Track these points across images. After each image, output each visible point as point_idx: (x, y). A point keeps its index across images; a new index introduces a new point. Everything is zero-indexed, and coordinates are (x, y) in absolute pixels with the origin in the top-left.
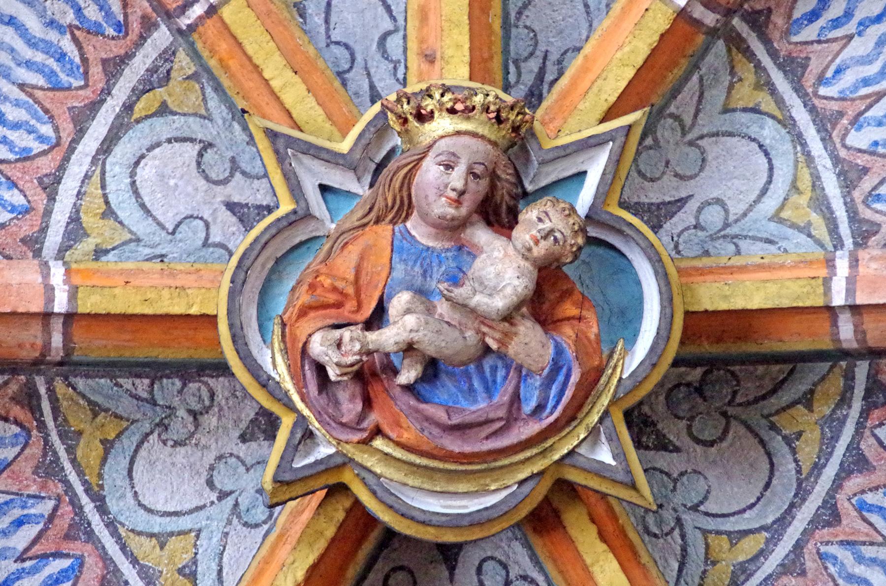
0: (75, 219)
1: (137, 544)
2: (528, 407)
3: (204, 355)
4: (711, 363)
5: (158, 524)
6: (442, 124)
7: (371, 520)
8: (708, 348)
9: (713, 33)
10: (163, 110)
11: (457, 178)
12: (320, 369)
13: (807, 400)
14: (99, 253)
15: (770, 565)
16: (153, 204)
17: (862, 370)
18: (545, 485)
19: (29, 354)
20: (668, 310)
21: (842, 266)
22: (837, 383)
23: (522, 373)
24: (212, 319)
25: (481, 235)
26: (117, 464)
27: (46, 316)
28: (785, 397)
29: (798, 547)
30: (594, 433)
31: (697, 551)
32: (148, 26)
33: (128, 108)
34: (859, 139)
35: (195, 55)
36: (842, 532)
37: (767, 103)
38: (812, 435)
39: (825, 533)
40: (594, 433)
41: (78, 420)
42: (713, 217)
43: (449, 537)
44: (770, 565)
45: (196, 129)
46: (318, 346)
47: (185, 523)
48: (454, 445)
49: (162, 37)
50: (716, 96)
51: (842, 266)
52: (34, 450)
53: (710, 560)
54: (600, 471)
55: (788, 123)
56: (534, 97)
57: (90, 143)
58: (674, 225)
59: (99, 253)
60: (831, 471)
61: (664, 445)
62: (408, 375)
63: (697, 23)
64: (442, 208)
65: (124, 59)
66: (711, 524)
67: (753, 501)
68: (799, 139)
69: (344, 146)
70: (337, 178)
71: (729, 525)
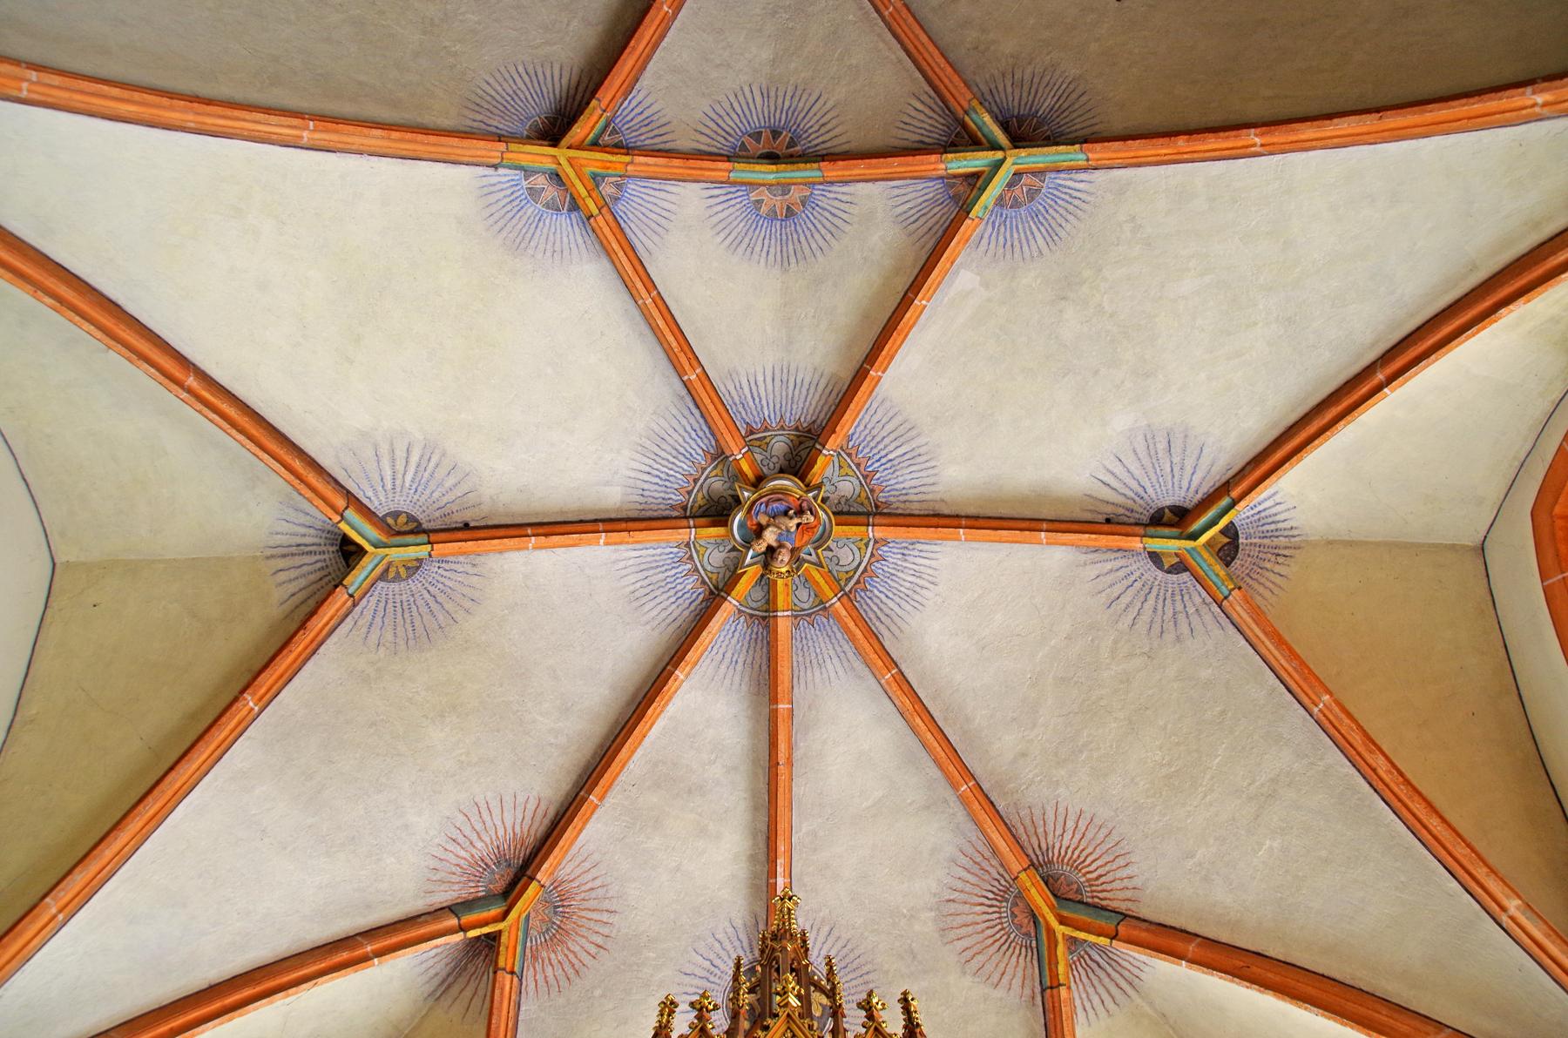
0: (867, 547)
1: (852, 474)
2: (763, 505)
3: (838, 517)
4: (722, 515)
5: (848, 478)
6: (784, 570)
7: (800, 479)
8: (723, 518)
9: (722, 590)
10: (847, 572)
11: (780, 558)
12: (812, 513)
13: (700, 507)
14: (861, 540)
15: (709, 469)
16: (782, 652)
17: (688, 514)
18: (760, 486)
19: (877, 517)
21: (692, 537)
22: (694, 511)
23: (765, 513)
24: (837, 525)
25: (775, 544)
26: (857, 492)
27: (873, 525)
28: (705, 508)
30: (749, 499)
32: (850, 591)
33: (855, 573)
34: (689, 566)
35: (840, 585)
37: (709, 574)
38: (699, 499)
40: (749, 499)
41: (866, 502)
42: (721, 549)
43: (782, 475)
44: (709, 469)
45: (838, 568)
46: (812, 519)
48: (780, 496)
49: (847, 589)
50: (721, 576)
51: (692, 537)
52: (875, 495)
53: (722, 470)
54: (747, 490)
55: (705, 570)
56: (762, 576)
57: (863, 565)
58: (730, 547)
59: (861, 540)
60: (695, 491)
61: (732, 496)
62: (791, 512)
63: (820, 444)
64: (784, 551)
65: (856, 584)
68: (702, 566)
69: (806, 565)
70: (808, 557)
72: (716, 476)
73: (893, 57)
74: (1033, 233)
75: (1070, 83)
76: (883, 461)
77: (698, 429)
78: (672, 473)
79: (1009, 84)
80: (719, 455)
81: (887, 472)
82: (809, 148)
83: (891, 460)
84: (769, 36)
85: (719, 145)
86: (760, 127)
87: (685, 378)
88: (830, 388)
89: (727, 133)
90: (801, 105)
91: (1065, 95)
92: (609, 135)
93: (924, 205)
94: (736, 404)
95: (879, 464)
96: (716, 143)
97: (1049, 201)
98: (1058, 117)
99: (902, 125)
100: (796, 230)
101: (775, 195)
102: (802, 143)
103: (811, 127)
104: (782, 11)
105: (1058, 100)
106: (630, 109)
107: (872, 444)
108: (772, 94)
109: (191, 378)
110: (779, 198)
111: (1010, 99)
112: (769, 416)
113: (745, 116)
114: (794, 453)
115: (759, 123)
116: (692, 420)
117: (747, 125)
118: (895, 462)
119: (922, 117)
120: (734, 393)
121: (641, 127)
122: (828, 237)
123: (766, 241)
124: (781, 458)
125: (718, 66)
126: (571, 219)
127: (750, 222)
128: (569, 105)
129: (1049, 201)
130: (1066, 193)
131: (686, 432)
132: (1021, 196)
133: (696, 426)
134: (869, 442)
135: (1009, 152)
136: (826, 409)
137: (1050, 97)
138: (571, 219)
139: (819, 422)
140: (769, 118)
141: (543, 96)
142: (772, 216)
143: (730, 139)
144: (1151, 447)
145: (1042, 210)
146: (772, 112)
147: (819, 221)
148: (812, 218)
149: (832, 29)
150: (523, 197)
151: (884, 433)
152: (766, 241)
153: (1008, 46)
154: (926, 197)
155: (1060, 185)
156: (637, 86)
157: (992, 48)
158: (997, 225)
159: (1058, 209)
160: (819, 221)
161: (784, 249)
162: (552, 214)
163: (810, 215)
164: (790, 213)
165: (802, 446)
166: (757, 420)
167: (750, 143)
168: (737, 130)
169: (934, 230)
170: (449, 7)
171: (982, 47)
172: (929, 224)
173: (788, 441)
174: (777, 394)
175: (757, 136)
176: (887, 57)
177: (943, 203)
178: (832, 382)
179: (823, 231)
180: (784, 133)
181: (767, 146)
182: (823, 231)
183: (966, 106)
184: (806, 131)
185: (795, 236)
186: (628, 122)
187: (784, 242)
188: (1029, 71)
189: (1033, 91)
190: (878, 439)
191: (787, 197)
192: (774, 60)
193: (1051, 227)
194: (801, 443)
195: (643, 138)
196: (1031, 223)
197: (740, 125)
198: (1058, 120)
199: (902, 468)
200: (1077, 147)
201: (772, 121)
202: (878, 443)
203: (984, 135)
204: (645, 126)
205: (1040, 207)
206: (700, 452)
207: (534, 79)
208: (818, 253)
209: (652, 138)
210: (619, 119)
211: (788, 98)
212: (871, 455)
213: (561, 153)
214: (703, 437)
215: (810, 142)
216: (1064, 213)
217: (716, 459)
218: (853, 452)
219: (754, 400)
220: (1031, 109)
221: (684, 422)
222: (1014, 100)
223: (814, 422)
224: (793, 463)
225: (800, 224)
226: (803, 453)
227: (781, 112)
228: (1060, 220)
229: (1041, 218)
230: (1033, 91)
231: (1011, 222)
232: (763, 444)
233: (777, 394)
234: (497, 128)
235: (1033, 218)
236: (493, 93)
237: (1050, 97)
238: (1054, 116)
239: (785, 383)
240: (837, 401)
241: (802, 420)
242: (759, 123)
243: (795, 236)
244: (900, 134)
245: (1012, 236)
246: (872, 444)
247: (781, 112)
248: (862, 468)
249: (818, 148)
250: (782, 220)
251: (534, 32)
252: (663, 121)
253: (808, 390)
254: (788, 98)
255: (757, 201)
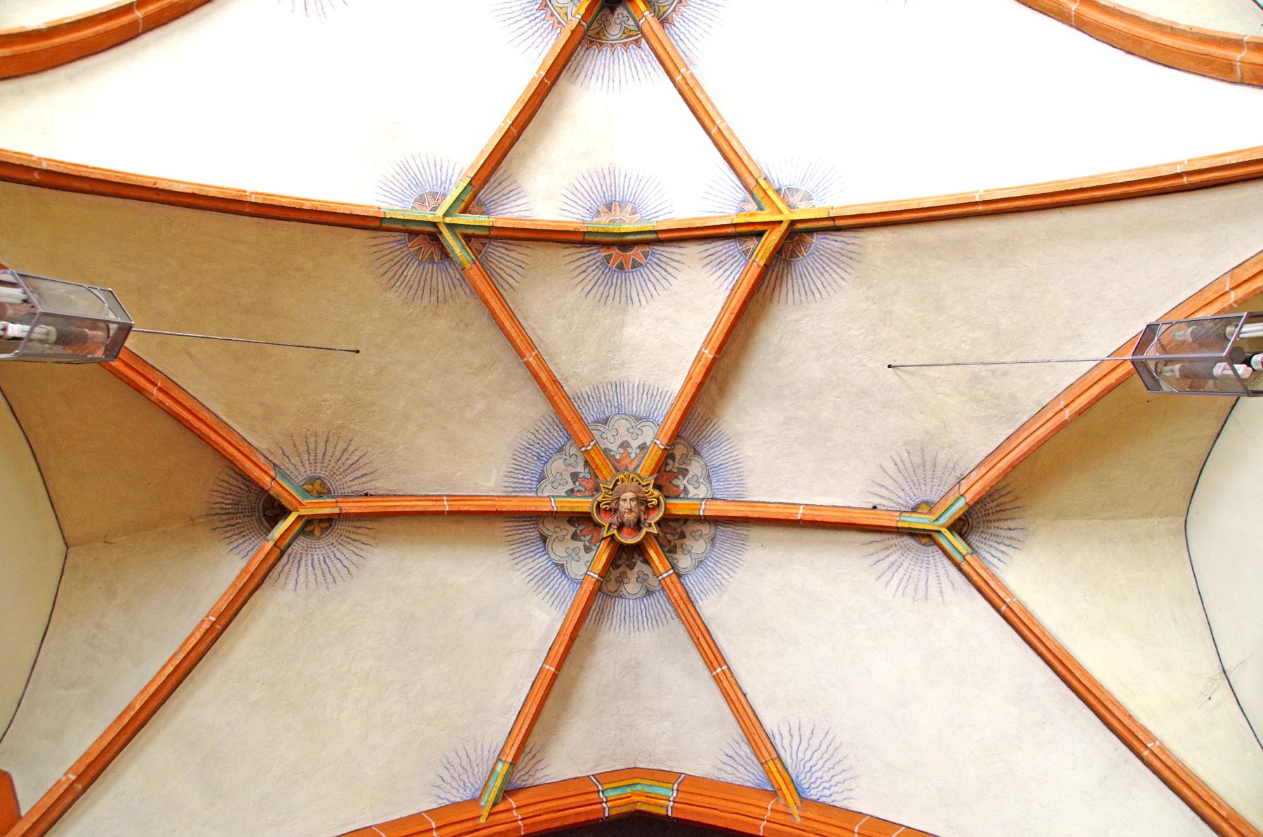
5: (560, 5)
20: (531, 368)
29: (675, 8)
31: (657, 9)
36: (682, 4)
39: (679, 5)
47: (565, 5)
53: (659, 10)
66: (659, 5)
67: (997, 559)
71: (663, 4)
72: (664, 6)
73: (530, 323)
74: (420, 172)
75: (394, 286)
76: (533, 17)
77: (679, 41)
78: (700, 7)
79: (441, 291)
80: (664, 21)
81: (530, 9)
82: (595, 254)
83: (527, 17)
84: (626, 345)
85: (664, 254)
86: (633, 272)
87: (703, 350)
88: (575, 74)
89: (659, 265)
90: (601, 289)
91: (397, 276)
92: (750, 249)
93: (505, 202)
94: (649, 61)
95: (536, 15)
96: (667, 255)
97: (408, 193)
98: (403, 258)
99: (523, 265)
100: (604, 193)
101: (621, 219)
102: (600, 258)
103: (593, 271)
104: (617, 366)
105: (402, 273)
106: (734, 273)
107: (542, 30)
108: (623, 299)
109: (1073, 9)
110: (618, 218)
111: (439, 279)
112: (623, 54)
113: (645, 280)
114: (602, 26)
115: (633, 275)
116: (683, 47)
117: (643, 273)
118: (523, 16)
119: (508, 271)
120: (651, 70)
121: (725, 260)
122: (579, 187)
123: (627, 185)
124: (613, 23)
125: (666, 318)
126: (779, 183)
127: (639, 198)
128: (781, 270)
129: (408, 193)
130: (395, 196)
131: (688, 38)
132: (430, 200)
133: (680, 43)
134: (544, 32)
135: (441, 220)
136: (579, 58)
137: (409, 276)
138: (779, 183)
139: (584, 49)
140: (626, 280)
141: (801, 275)
142: (622, 205)
143: (656, 261)
144: (320, 8)
145: (412, 187)
146: (623, 285)
147: (586, 199)
148: (592, 201)
149: (577, 350)
150: (815, 194)
151: (532, 39)
152: (627, 185)
153: (442, 325)
154: (503, 207)
155: (400, 202)
156: (728, 292)
157: (454, 324)
158: (448, 182)
159: (400, 186)
160: (586, 199)
161: (613, 180)
162: (794, 185)
163: (594, 204)
164: (609, 206)
165: (596, 31)
166: (632, 51)
167: (641, 259)
168: (650, 268)
169: (497, 183)
170: (872, 338)
171: (462, 326)
172: (500, 188)
173: (608, 35)
174: (617, 72)
175: (636, 265)
176: (536, 322)
177: (490, 202)
178: (574, 78)
179: (583, 191)
180: (614, 267)
181: (627, 258)
182: (583, 191)
183: (474, 266)
184: (597, 268)
185: (604, 189)
186: (735, 262)
187: (613, 185)
188: (426, 301)
189: (422, 283)
190: (538, 34)
191: (612, 218)
192: (623, 326)
193: (406, 174)
194: (598, 33)
195: (724, 251)
196: (421, 180)
197: (648, 273)
198: (402, 255)
199: (518, 11)
200: (388, 216)
201: (623, 278)
202: (537, 31)
203: (461, 241)
204: (722, 262)
205: (414, 189)
206: (676, 24)
207: (807, 289)
208: (587, 176)
209: (717, 252)
210: (742, 263)
211: (611, 296)
212: (542, 22)
213: (787, 216)
214: (674, 35)
215: (594, 259)
216: (396, 182)
217: (664, 19)
218: (556, 25)
219: (635, 66)
220: (424, 268)
221: (689, 45)
222: (439, 277)
223: (588, 49)
224: (604, 19)
225: (601, 197)
226: (595, 25)
227: (616, 284)
228: (399, 178)
229: (414, 181)
230: (422, 283)
231: (437, 181)
232: (627, 33)
233: (617, 72)
234: (836, 241)
235: (420, 182)
236: (839, 270)
237: (409, 276)
238: (405, 259)
239: (611, 78)
240: (569, 64)
241: (597, 51)
242: (633, 275)
243: (604, 189)
244: (524, 258)
245: (436, 172)
246: (542, 30)
247: (616, 284)
248: (549, 13)
249: (588, 253)
250: (615, 201)
251: (808, 328)
252: (708, 267)
253: (593, 73)
254: (611, 296)
255: (634, 213)
